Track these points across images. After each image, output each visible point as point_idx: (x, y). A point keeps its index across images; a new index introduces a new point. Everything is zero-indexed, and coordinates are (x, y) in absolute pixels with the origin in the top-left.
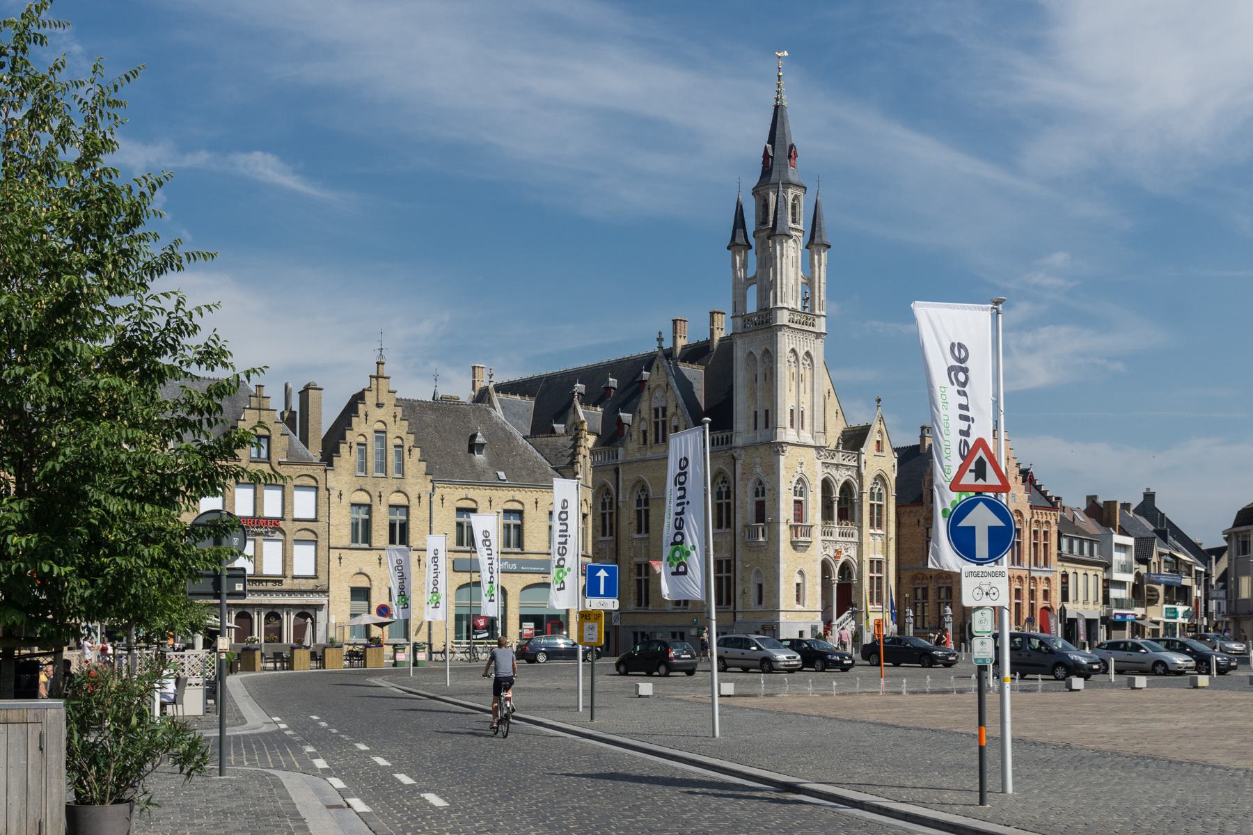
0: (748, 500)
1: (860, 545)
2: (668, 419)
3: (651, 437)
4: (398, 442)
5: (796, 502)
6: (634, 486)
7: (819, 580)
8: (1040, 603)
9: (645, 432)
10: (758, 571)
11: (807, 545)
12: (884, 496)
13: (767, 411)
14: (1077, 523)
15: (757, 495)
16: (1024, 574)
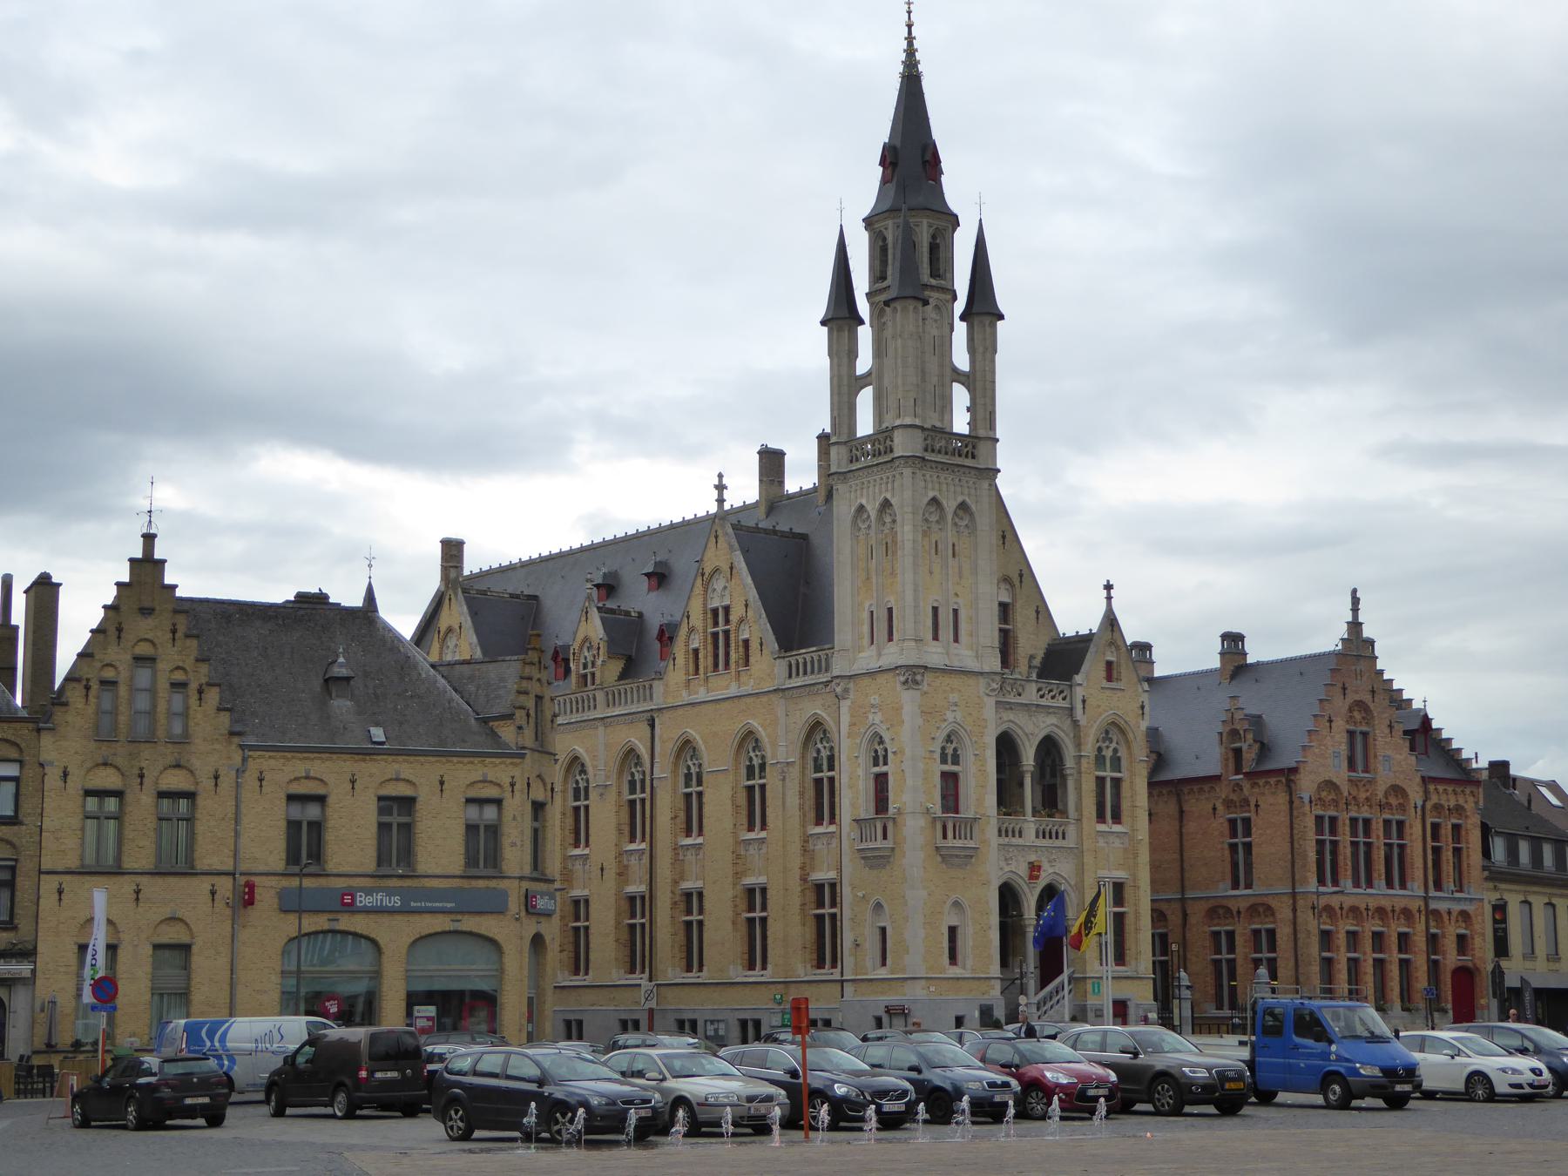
0: (860, 772)
1: (1078, 852)
2: (732, 627)
3: (705, 660)
4: (179, 676)
5: (944, 775)
7: (995, 919)
8: (1451, 958)
9: (696, 651)
10: (878, 906)
11: (969, 856)
12: (1124, 763)
14: (1535, 809)
16: (1415, 905)
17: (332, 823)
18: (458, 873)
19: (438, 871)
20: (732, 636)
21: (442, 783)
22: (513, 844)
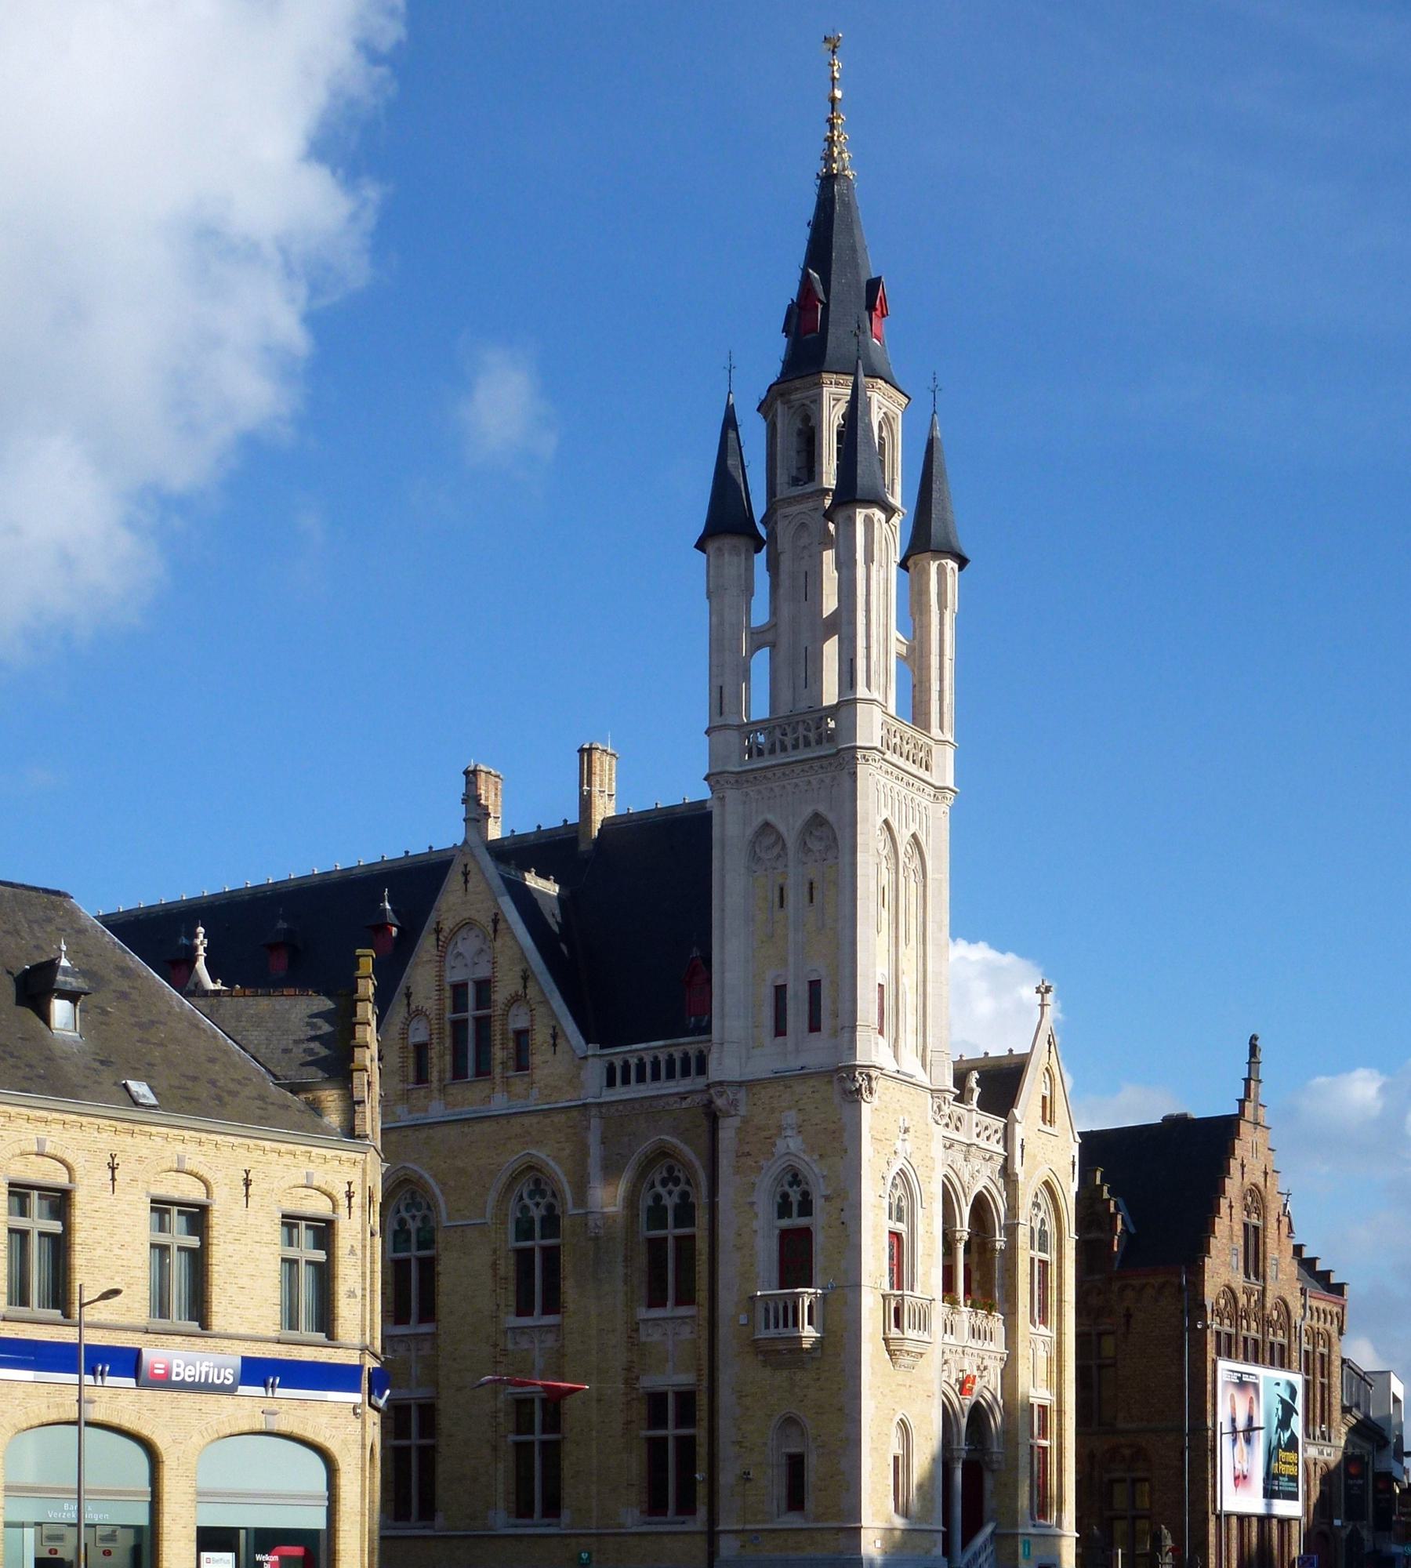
3: (440, 1062)
6: (514, 1179)
9: (421, 1050)
13: (815, 986)
15: (784, 1210)
17: (79, 1237)
18: (273, 1334)
19: (243, 1330)
20: (497, 1027)
21: (247, 1183)
22: (351, 1294)
